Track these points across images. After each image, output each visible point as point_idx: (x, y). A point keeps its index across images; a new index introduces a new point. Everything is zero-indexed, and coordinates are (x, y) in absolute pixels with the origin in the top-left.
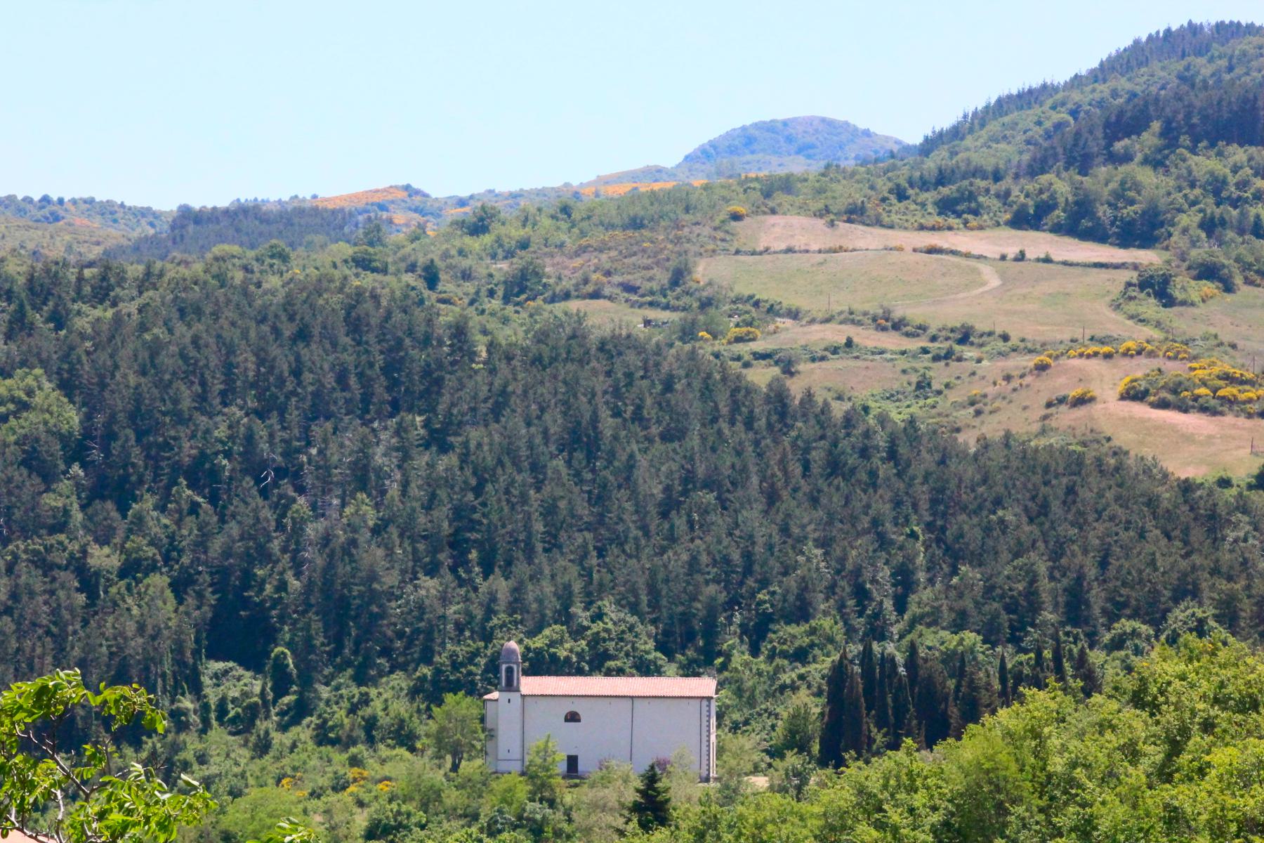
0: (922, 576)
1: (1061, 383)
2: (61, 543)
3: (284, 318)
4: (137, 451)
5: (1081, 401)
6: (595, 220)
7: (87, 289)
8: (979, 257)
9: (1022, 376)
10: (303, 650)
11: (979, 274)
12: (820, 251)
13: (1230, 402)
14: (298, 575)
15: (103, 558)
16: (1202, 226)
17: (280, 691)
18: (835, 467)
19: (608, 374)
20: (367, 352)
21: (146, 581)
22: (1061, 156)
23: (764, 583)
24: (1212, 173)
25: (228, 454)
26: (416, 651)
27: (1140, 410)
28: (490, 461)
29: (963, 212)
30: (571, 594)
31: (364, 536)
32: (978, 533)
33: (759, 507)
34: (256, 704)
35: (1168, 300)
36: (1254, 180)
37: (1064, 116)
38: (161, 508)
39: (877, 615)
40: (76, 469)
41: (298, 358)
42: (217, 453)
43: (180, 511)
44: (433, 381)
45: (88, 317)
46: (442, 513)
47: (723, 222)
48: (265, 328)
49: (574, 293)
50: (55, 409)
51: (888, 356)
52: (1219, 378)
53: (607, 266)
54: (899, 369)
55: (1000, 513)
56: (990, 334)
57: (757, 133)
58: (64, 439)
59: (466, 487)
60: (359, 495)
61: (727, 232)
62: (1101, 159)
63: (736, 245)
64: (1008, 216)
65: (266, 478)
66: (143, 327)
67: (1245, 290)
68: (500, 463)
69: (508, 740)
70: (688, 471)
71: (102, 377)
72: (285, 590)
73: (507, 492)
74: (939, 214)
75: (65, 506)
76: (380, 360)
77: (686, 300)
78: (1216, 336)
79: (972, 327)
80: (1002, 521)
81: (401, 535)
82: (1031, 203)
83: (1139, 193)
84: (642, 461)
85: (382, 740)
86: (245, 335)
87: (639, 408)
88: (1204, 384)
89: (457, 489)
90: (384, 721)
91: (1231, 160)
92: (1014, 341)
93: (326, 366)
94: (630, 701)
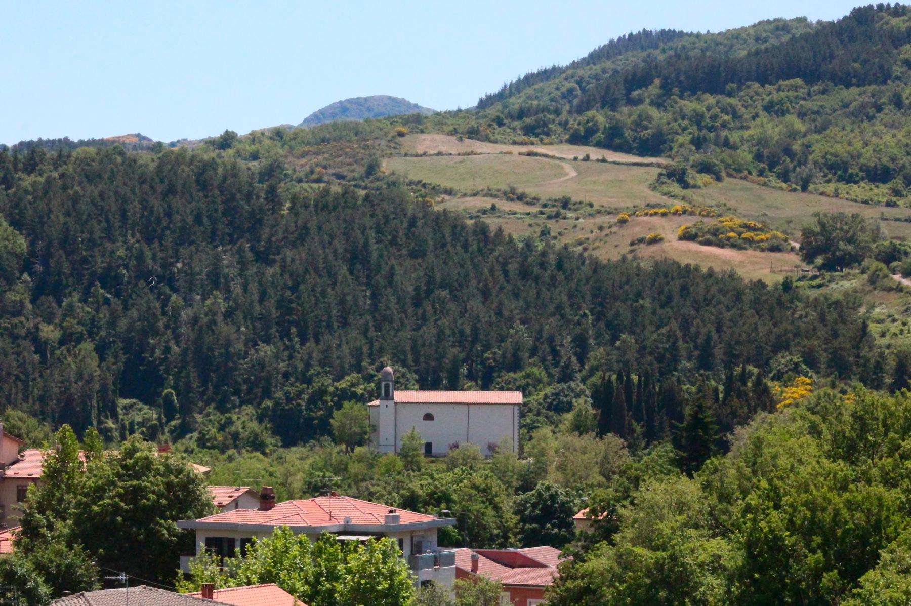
0: (592, 342)
1: (637, 230)
2: (21, 322)
3: (157, 180)
4: (66, 265)
5: (655, 240)
6: (299, 140)
7: (20, 166)
8: (561, 159)
9: (610, 227)
10: (184, 392)
11: (562, 168)
12: (459, 155)
13: (750, 241)
14: (177, 343)
15: (49, 332)
16: (692, 142)
17: (170, 418)
18: (525, 273)
19: (372, 216)
20: (213, 202)
21: (79, 346)
22: (598, 100)
23: (487, 347)
24: (695, 111)
25: (126, 267)
26: (258, 391)
27: (693, 246)
28: (300, 271)
29: (540, 134)
30: (362, 353)
31: (219, 319)
32: (629, 315)
33: (479, 298)
34: (156, 425)
35: (686, 186)
36: (721, 115)
37: (572, 84)
38: (84, 301)
39: (567, 366)
40: (26, 276)
41: (169, 206)
42: (119, 266)
43: (97, 302)
44: (256, 220)
45: (27, 181)
46: (271, 303)
47: (394, 137)
48: (146, 187)
49: (305, 180)
50: (11, 238)
51: (519, 216)
52: (741, 226)
53: (324, 163)
54: (527, 223)
55: (641, 302)
56: (581, 203)
57: (348, 106)
58: (18, 256)
59: (285, 287)
60: (214, 292)
61: (396, 143)
62: (624, 102)
63: (403, 152)
64: (567, 137)
65: (151, 282)
66: (65, 188)
67: (727, 180)
68: (306, 271)
69: (386, 432)
70: (430, 277)
71: (41, 217)
72: (169, 353)
73: (313, 290)
74: (525, 135)
75: (21, 300)
76: (221, 208)
77: (378, 184)
78: (725, 205)
79: (570, 199)
80: (642, 307)
81: (245, 318)
82: (581, 128)
83: (650, 122)
84: (399, 271)
85: (244, 447)
86: (133, 191)
87: (395, 237)
88: (732, 230)
89: (279, 288)
90: (244, 434)
91: (706, 103)
92: (596, 207)
93: (188, 211)
94: (466, 407)
